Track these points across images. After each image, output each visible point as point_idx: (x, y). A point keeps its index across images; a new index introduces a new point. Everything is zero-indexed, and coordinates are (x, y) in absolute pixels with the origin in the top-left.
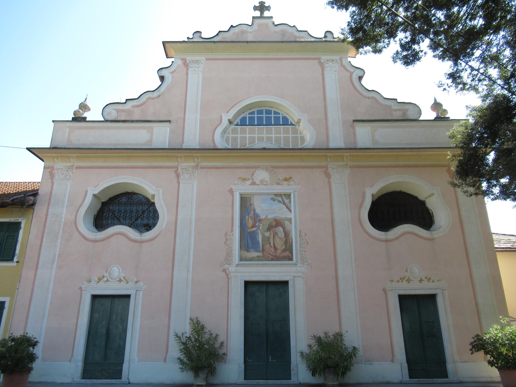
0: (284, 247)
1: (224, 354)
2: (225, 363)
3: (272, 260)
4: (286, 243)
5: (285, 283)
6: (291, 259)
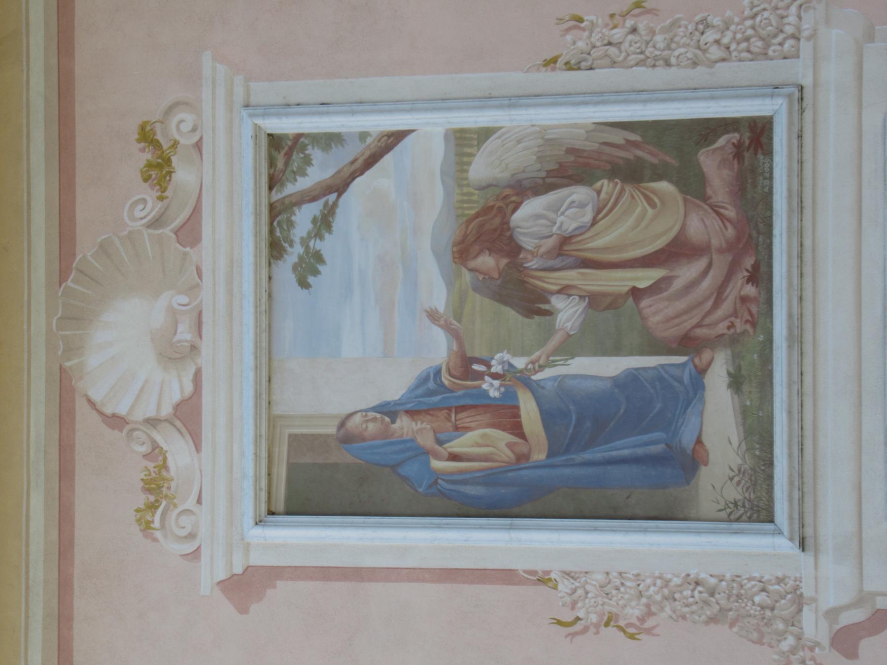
3: (761, 275)
4: (632, 173)
6: (757, 134)
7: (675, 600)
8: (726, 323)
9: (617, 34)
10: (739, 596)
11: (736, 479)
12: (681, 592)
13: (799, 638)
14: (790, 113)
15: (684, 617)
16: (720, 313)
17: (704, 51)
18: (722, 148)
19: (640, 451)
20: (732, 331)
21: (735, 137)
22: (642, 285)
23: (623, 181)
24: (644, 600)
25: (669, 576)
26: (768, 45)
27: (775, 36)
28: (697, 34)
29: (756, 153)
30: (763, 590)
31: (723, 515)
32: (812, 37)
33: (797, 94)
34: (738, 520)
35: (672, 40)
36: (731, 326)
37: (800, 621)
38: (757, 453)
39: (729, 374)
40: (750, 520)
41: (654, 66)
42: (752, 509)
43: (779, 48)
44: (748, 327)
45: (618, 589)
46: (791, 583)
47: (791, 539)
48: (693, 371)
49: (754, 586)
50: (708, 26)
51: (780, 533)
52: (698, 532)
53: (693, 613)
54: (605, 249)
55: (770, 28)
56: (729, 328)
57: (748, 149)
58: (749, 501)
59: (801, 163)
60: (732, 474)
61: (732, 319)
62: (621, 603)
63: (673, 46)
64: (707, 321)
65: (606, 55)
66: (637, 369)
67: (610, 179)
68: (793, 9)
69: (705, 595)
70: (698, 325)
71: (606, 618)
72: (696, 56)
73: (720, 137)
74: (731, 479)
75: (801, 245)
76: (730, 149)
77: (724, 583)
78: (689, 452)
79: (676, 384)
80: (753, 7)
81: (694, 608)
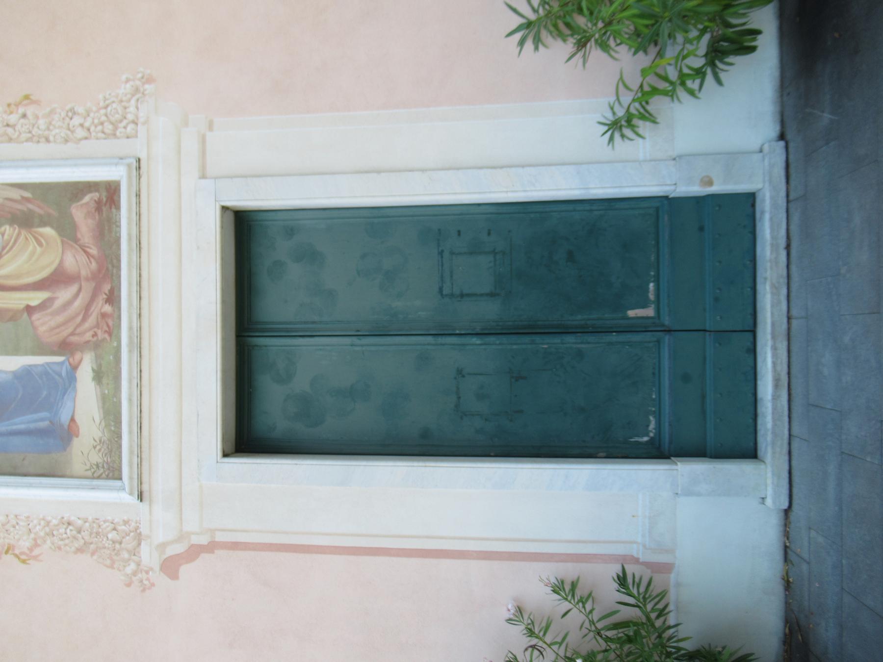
0: (48, 231)
1: (622, 580)
2: (666, 568)
3: (113, 298)
4: (25, 221)
5: (245, 230)
6: (110, 193)
7: (53, 535)
8: (91, 333)
9: (13, 119)
10: (98, 533)
11: (98, 447)
12: (58, 530)
13: (138, 564)
14: (129, 177)
15: (59, 548)
16: (87, 325)
17: (73, 132)
18: (87, 203)
19: (32, 426)
20: (95, 338)
21: (95, 195)
22: (34, 303)
23: (19, 226)
24: (32, 536)
25: (49, 518)
26: (116, 128)
27: (121, 121)
28: (68, 119)
29: (111, 208)
30: (114, 529)
31: (89, 473)
32: (145, 123)
33: (135, 164)
34: (99, 477)
35: (50, 123)
36: (95, 335)
37: (139, 552)
38: (113, 428)
39: (93, 370)
40: (108, 478)
41: (38, 142)
42: (109, 469)
43: (123, 130)
44: (106, 336)
45: (14, 527)
46: (133, 524)
47: (131, 494)
48: (69, 367)
49: (108, 526)
50: (75, 113)
51: (124, 489)
52: (67, 487)
53: (66, 545)
54: (7, 277)
55: (117, 116)
56: (93, 336)
57: (105, 205)
58: (107, 463)
59: (139, 215)
60: (95, 444)
61: (96, 330)
62: (16, 537)
63: (51, 127)
64: (78, 331)
65: (6, 134)
66: (30, 366)
67: (11, 225)
68: (133, 102)
69: (74, 532)
70: (73, 334)
71: (6, 548)
72: (67, 135)
73: (85, 195)
74: (95, 447)
75: (140, 276)
76: (93, 205)
77: (87, 524)
78: (66, 427)
79: (57, 377)
80: (105, 99)
81: (67, 541)
